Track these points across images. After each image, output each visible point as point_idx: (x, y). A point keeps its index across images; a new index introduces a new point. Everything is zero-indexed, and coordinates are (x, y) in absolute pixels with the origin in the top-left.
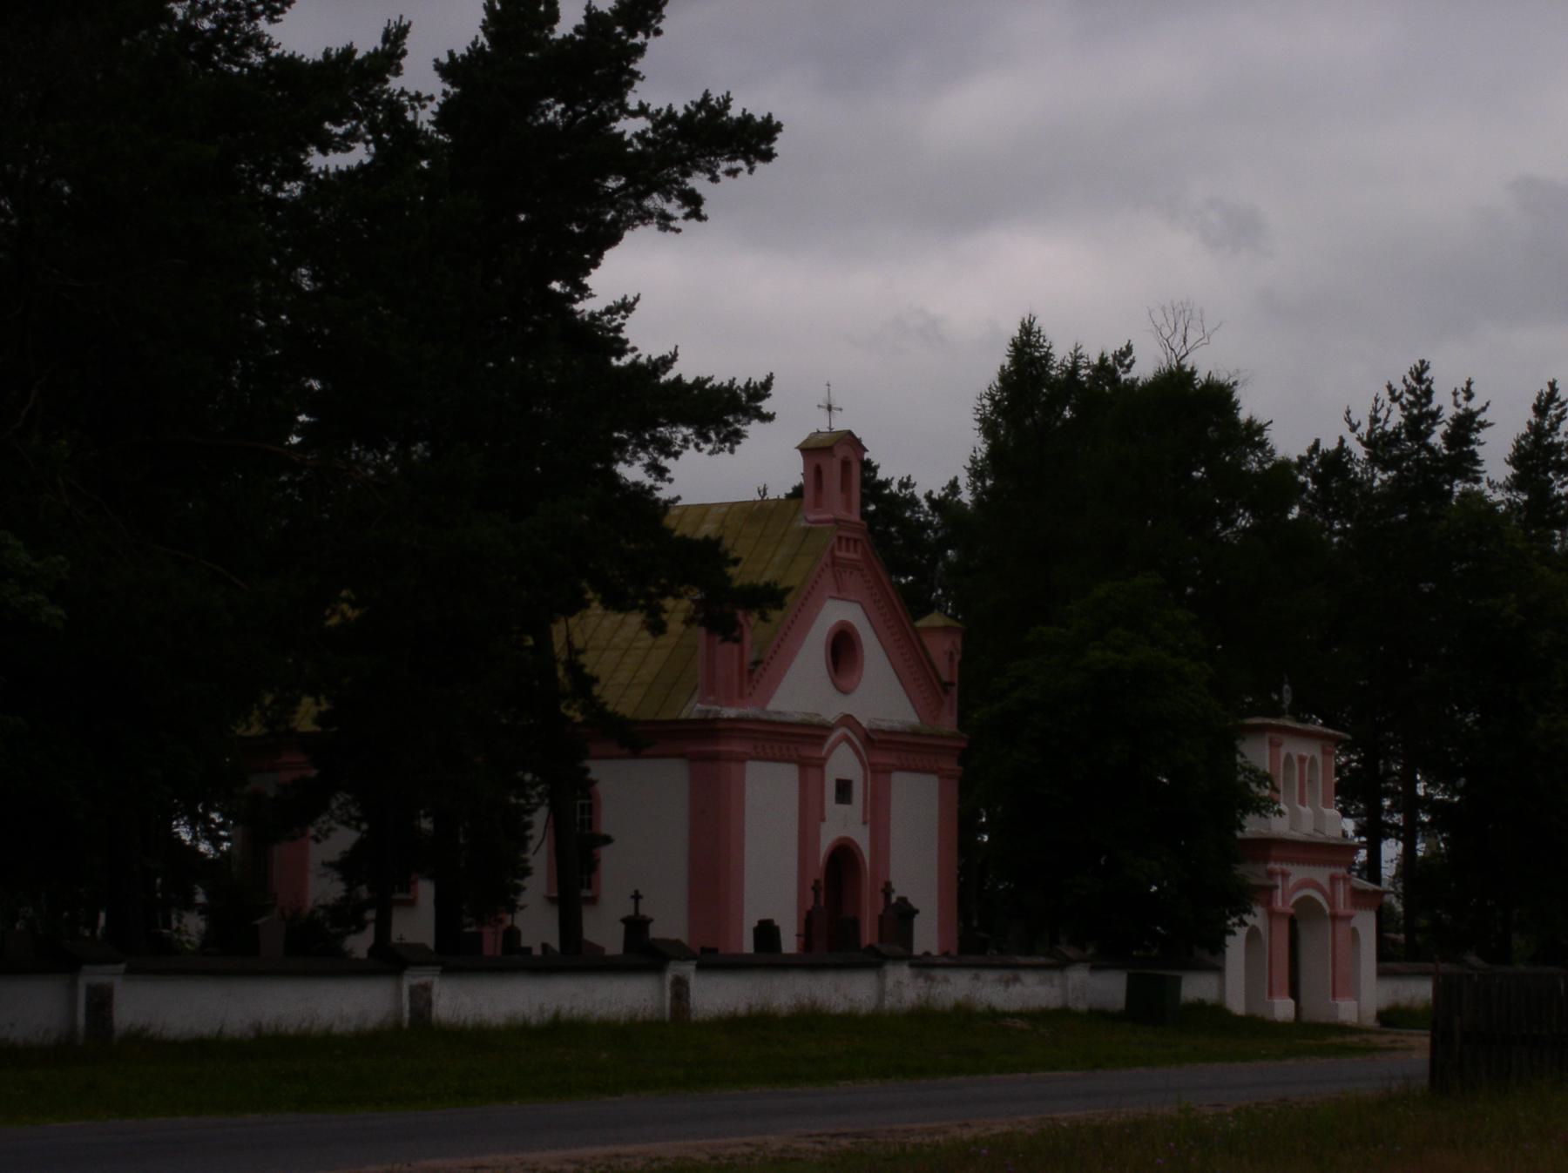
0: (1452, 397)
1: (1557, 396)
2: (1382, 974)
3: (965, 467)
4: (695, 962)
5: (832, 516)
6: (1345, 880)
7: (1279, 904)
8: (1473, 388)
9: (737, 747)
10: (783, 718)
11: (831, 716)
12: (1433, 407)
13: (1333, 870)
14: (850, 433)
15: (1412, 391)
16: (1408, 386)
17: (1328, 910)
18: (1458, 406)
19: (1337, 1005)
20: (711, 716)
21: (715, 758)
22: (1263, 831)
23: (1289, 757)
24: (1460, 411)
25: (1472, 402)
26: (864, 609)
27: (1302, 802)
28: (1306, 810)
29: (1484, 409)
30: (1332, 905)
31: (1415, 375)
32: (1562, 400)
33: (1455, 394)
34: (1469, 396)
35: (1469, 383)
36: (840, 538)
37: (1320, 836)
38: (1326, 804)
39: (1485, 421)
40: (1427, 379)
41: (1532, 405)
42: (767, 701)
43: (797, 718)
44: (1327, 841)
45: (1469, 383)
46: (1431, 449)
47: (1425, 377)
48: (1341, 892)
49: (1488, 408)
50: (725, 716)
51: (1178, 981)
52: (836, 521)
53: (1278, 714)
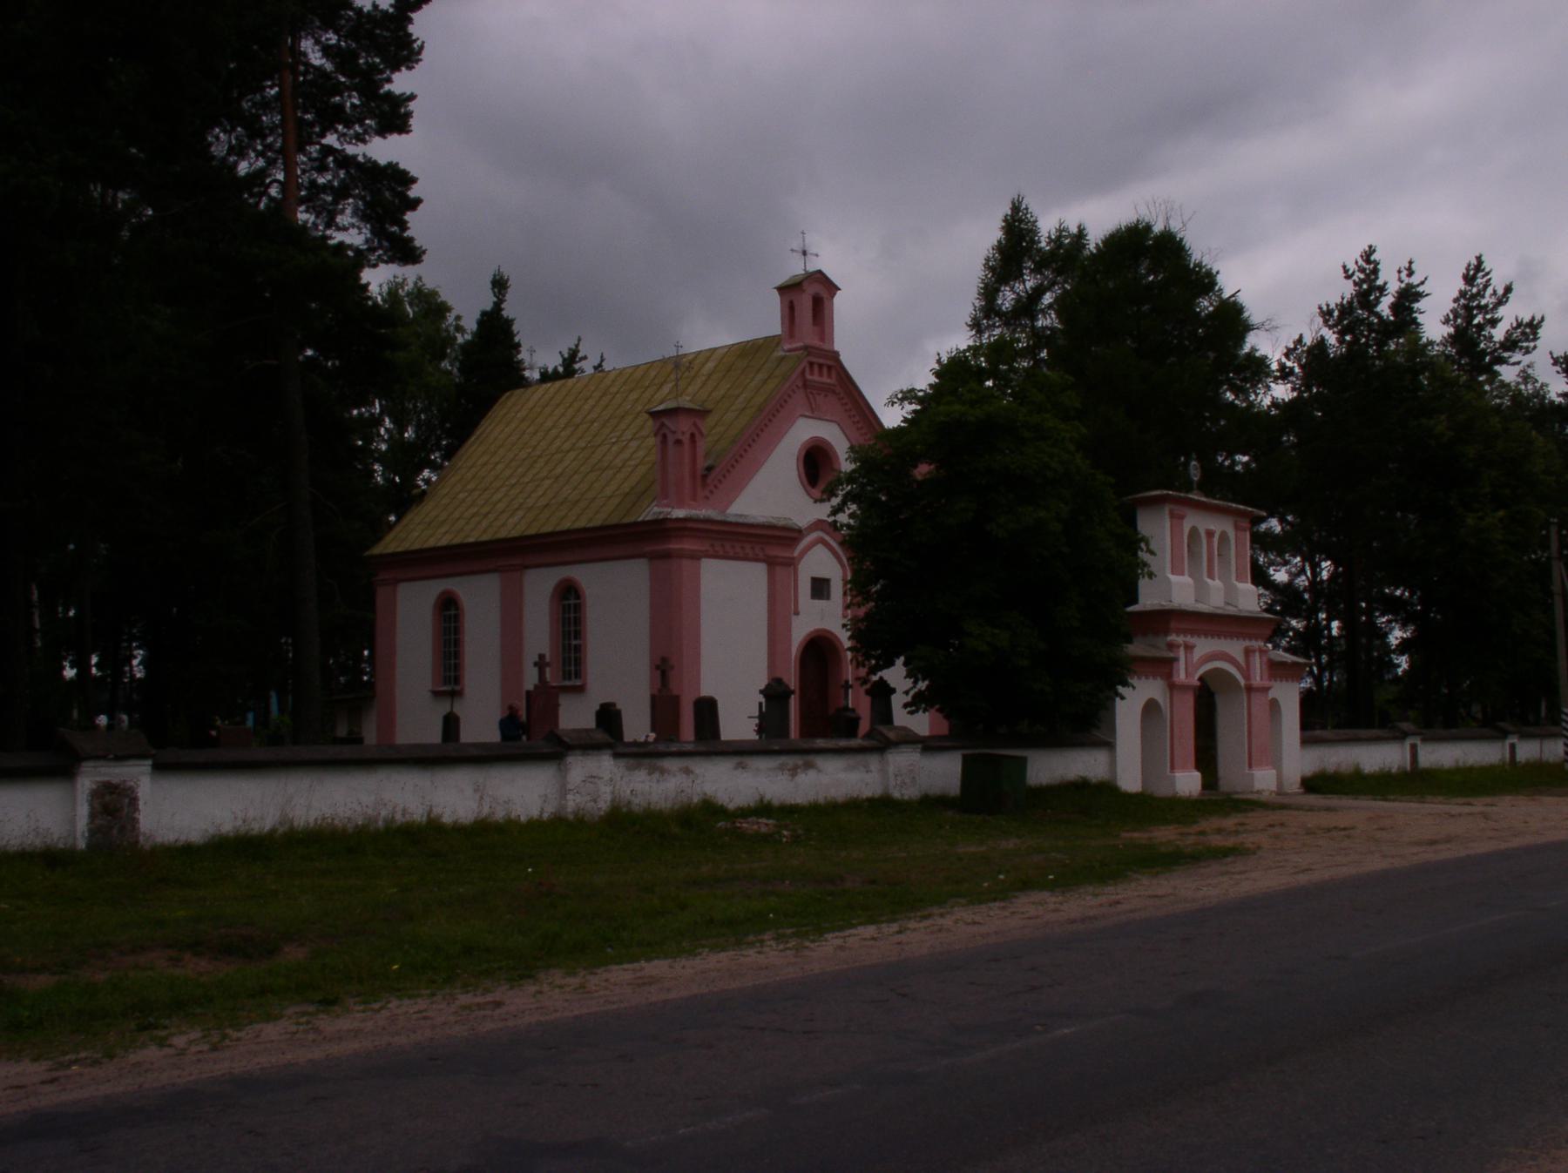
0: (1397, 275)
1: (1482, 267)
2: (1306, 742)
3: (966, 323)
4: (150, 762)
5: (802, 344)
6: (1262, 652)
7: (1181, 676)
8: (1414, 266)
9: (688, 545)
10: (746, 521)
11: (802, 521)
12: (1379, 282)
13: (1247, 643)
14: (820, 272)
15: (1362, 270)
16: (1359, 267)
17: (1242, 682)
18: (1402, 282)
19: (1253, 774)
20: (661, 517)
21: (667, 555)
22: (1164, 603)
23: (1194, 532)
24: (1403, 285)
25: (1413, 277)
26: (841, 428)
27: (1211, 576)
28: (1216, 584)
29: (1422, 283)
30: (1247, 677)
31: (1364, 258)
32: (1487, 270)
33: (1399, 272)
34: (1411, 273)
35: (1411, 263)
36: (811, 364)
37: (1230, 608)
38: (1240, 578)
39: (1424, 292)
40: (1375, 261)
41: (1461, 274)
42: (727, 507)
43: (761, 520)
44: (1238, 614)
45: (1411, 263)
46: (1378, 316)
47: (1372, 258)
48: (1257, 661)
49: (1426, 282)
50: (674, 517)
51: (1023, 762)
52: (806, 348)
53: (1189, 490)
